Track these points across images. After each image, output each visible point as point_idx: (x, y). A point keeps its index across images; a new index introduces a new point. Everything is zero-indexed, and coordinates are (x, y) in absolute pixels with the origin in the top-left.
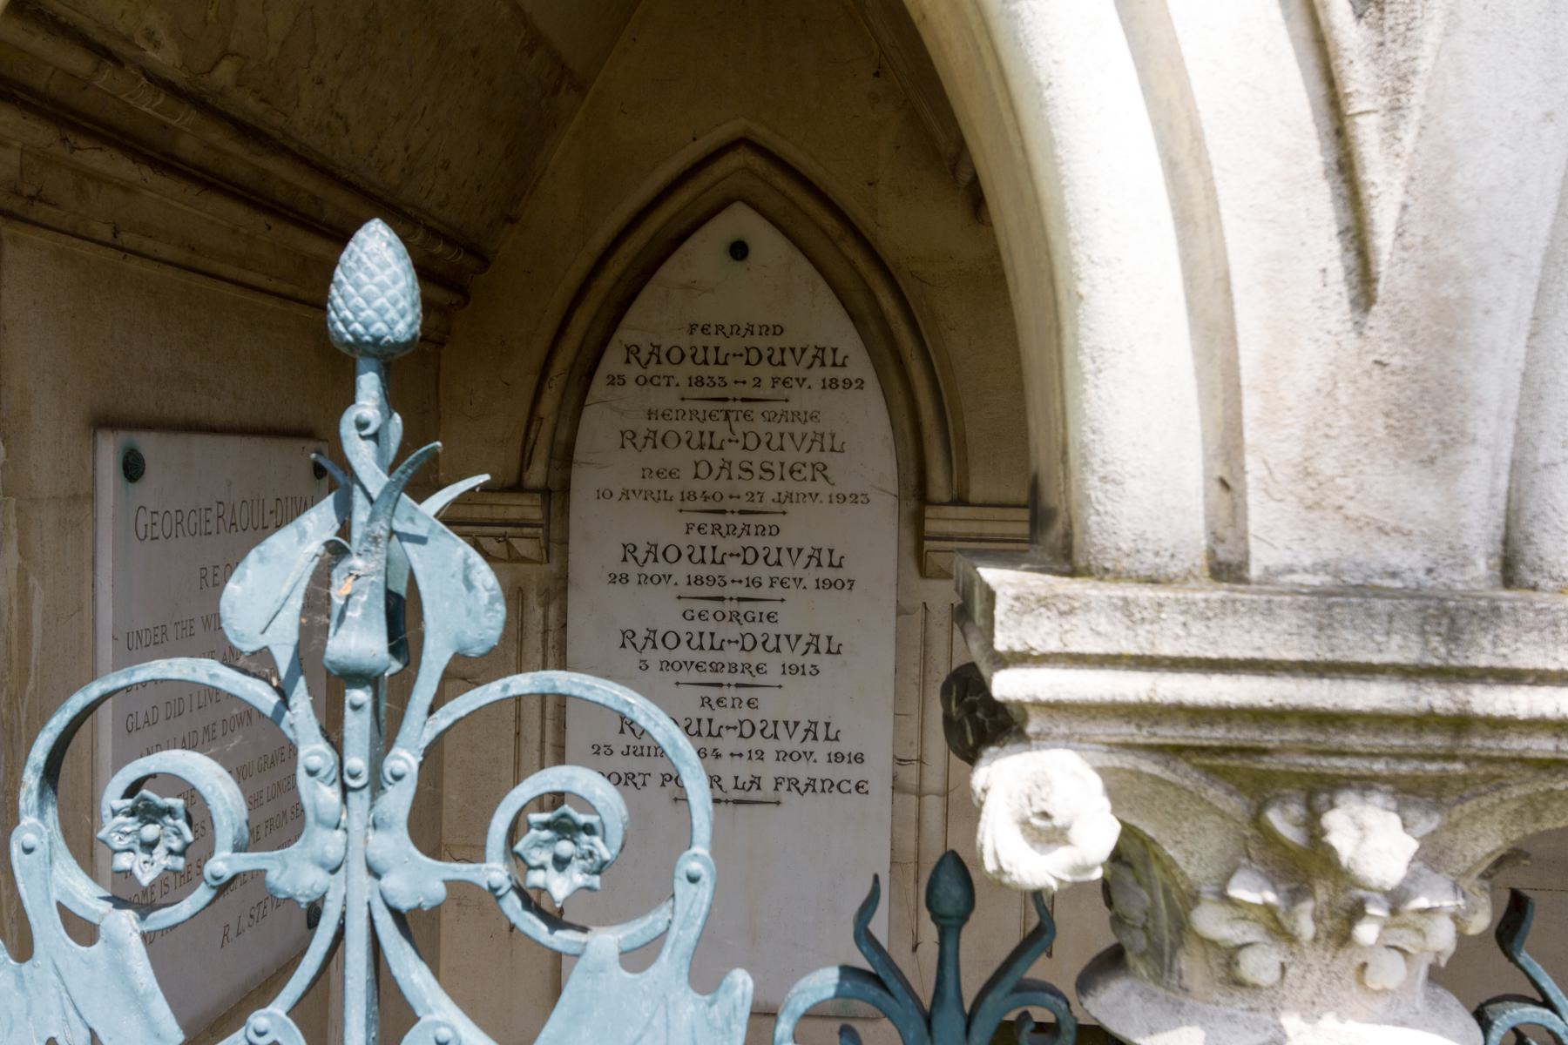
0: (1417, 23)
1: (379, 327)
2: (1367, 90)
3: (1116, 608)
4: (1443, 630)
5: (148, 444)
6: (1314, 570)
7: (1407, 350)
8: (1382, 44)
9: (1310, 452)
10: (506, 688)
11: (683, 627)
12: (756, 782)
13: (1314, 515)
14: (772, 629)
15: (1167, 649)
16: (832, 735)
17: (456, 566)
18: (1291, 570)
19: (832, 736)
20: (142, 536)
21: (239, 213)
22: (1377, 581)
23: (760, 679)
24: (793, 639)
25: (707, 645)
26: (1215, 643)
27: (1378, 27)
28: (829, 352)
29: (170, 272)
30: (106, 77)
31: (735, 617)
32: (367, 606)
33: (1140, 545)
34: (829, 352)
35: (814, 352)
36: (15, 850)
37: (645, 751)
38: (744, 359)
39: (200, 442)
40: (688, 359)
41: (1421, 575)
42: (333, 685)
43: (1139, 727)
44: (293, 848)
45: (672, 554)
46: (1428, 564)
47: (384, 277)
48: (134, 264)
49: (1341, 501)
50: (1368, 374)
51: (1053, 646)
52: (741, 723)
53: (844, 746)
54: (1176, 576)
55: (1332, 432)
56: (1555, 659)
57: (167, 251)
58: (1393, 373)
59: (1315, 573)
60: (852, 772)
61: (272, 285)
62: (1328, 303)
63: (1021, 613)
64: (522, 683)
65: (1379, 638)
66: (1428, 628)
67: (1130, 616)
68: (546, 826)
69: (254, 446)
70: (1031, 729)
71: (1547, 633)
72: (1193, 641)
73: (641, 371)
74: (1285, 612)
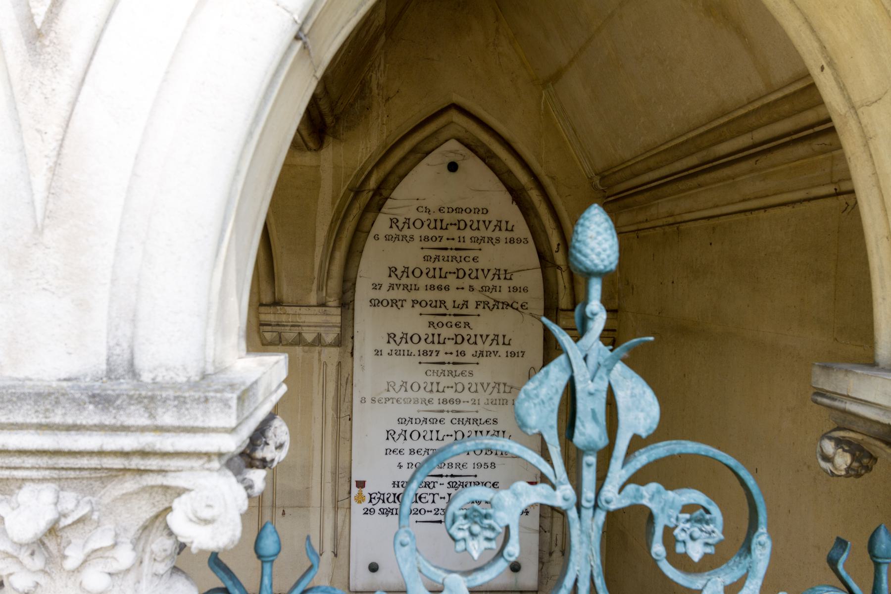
11: (424, 266)
12: (466, 304)
14: (473, 265)
16: (509, 228)
19: (506, 342)
23: (464, 311)
24: (486, 272)
25: (435, 389)
28: (502, 272)
31: (454, 258)
34: (502, 272)
35: (496, 223)
37: (402, 353)
38: (454, 389)
40: (424, 275)
45: (417, 273)
52: (459, 221)
53: (514, 348)
60: (520, 297)
73: (398, 232)
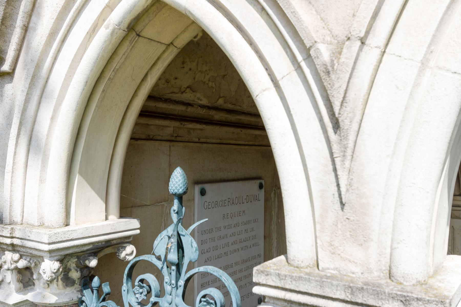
0: (349, 135)
1: (176, 191)
2: (337, 152)
3: (277, 275)
4: (350, 291)
5: (207, 187)
6: (334, 269)
7: (354, 215)
8: (341, 140)
9: (332, 240)
10: (199, 269)
13: (333, 256)
15: (287, 287)
17: (190, 242)
18: (328, 269)
20: (206, 208)
21: (232, 129)
22: (349, 274)
26: (297, 287)
27: (340, 135)
29: (215, 145)
30: (190, 109)
32: (174, 249)
33: (295, 259)
36: (123, 291)
39: (222, 185)
41: (360, 274)
42: (170, 265)
43: (288, 304)
44: (163, 298)
46: (362, 272)
47: (177, 180)
48: (205, 145)
49: (340, 253)
50: (345, 221)
51: (264, 282)
54: (303, 267)
55: (337, 235)
56: (378, 303)
57: (214, 141)
58: (351, 221)
59: (334, 270)
61: (246, 143)
62: (335, 203)
63: (259, 273)
64: (202, 269)
65: (334, 291)
66: (346, 290)
67: (280, 277)
68: (205, 301)
69: (240, 184)
70: (266, 300)
71: (376, 296)
72: (293, 285)
74: (313, 281)
